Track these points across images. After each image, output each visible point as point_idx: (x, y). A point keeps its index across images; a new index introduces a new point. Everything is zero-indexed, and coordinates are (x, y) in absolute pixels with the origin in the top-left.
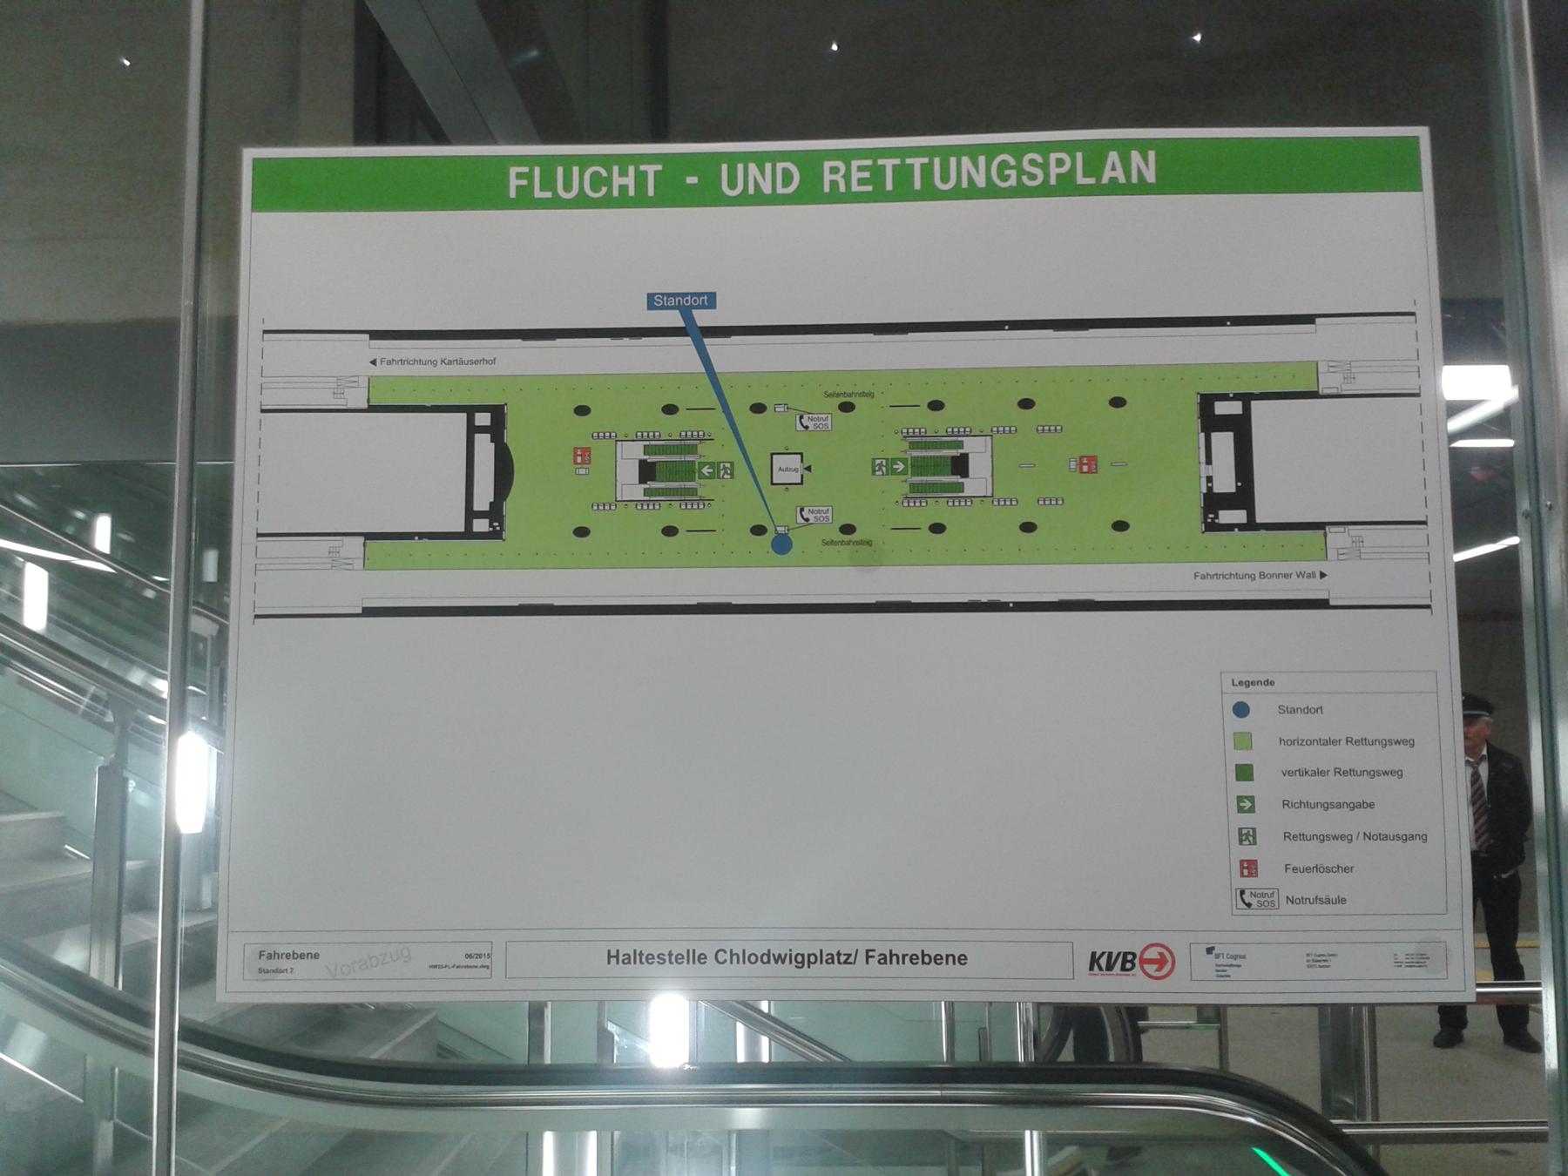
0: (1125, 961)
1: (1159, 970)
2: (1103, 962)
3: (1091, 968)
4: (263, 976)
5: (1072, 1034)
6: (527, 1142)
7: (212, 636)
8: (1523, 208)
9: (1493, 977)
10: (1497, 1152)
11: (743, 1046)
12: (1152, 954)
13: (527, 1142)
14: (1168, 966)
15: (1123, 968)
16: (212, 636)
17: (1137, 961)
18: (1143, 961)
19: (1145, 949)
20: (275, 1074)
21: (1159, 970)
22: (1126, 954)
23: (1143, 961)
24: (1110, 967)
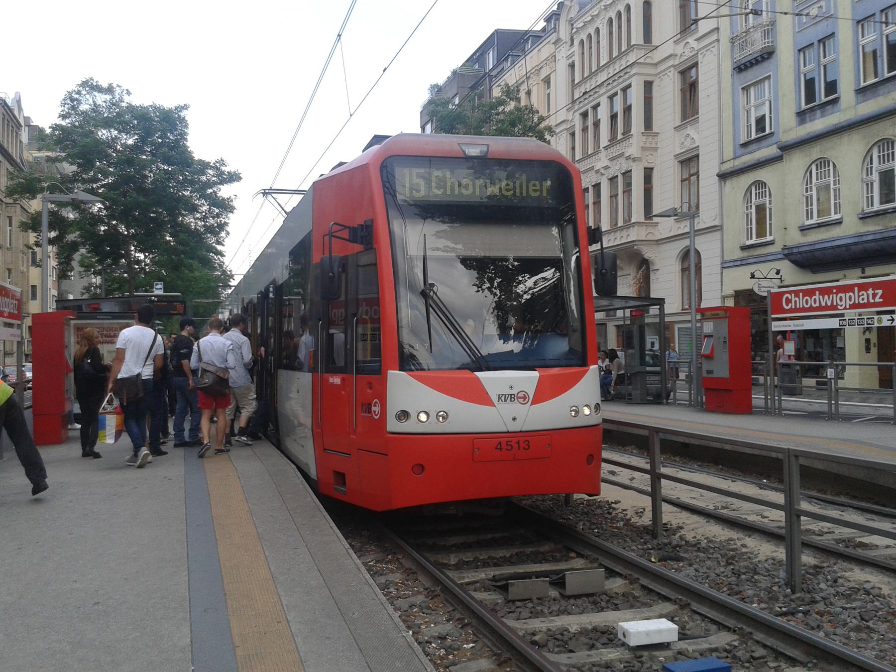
0: (511, 398)
1: (524, 401)
2: (503, 398)
3: (499, 401)
4: (752, 75)
5: (33, 437)
6: (723, 252)
7: (477, 278)
8: (866, 41)
9: (878, 386)
10: (569, 658)
11: (177, 443)
12: (521, 395)
13: (723, 252)
14: (527, 399)
15: (511, 401)
16: (477, 278)
17: (515, 398)
18: (518, 398)
19: (519, 393)
20: (554, 568)
21: (524, 401)
22: (511, 395)
23: (518, 398)
24: (506, 400)
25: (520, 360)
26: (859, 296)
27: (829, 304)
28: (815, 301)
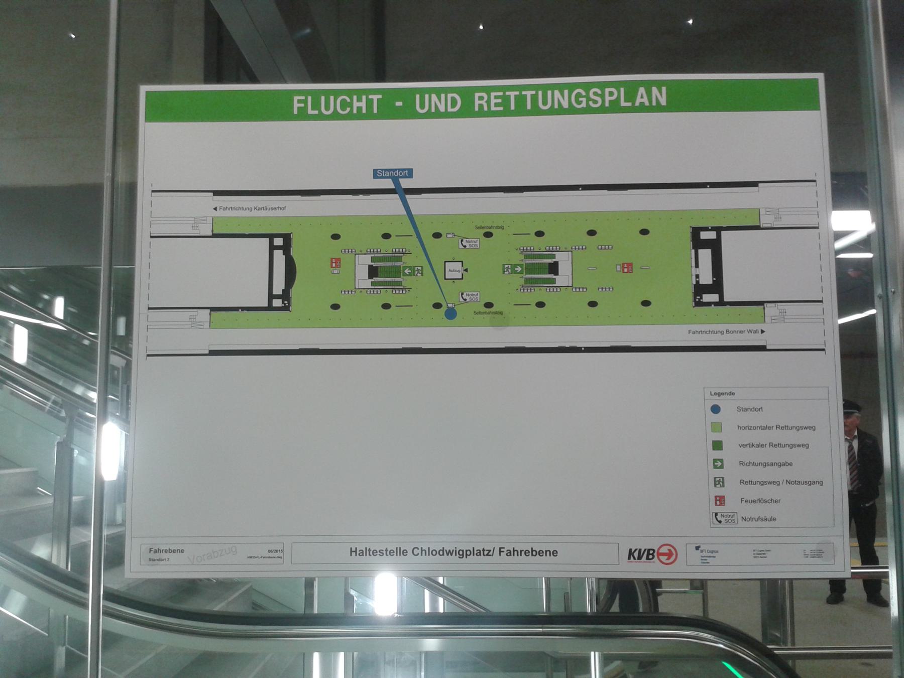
0: (648, 554)
1: (668, 559)
2: (636, 555)
3: (629, 558)
4: (151, 562)
5: (618, 596)
6: (304, 658)
7: (122, 367)
10: (863, 664)
12: (664, 550)
13: (304, 658)
14: (674, 557)
15: (648, 558)
16: (122, 367)
17: (655, 554)
18: (659, 554)
19: (660, 547)
21: (668, 559)
22: (649, 550)
23: (659, 554)
24: (640, 558)
25: (189, 558)
26: (385, 173)
27: (565, 105)
28: (396, 174)
